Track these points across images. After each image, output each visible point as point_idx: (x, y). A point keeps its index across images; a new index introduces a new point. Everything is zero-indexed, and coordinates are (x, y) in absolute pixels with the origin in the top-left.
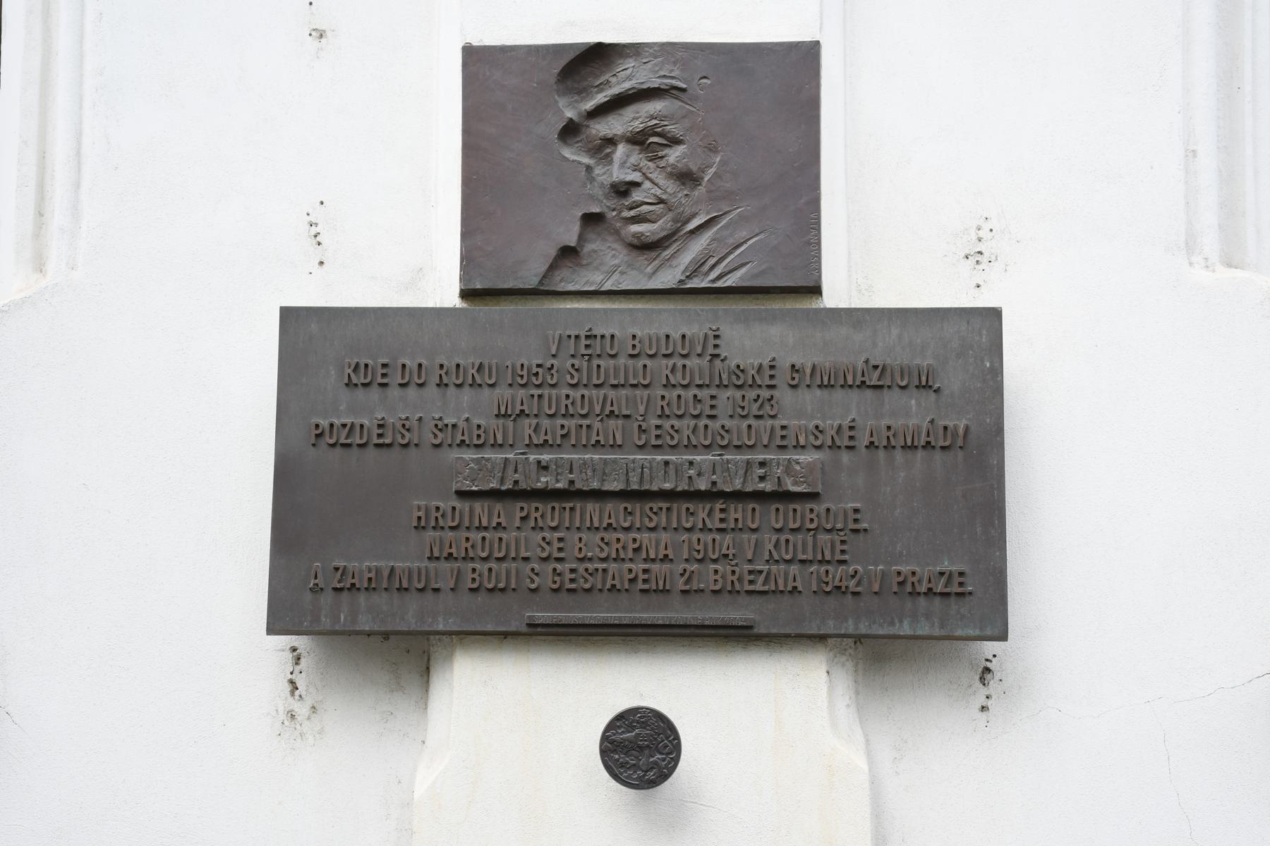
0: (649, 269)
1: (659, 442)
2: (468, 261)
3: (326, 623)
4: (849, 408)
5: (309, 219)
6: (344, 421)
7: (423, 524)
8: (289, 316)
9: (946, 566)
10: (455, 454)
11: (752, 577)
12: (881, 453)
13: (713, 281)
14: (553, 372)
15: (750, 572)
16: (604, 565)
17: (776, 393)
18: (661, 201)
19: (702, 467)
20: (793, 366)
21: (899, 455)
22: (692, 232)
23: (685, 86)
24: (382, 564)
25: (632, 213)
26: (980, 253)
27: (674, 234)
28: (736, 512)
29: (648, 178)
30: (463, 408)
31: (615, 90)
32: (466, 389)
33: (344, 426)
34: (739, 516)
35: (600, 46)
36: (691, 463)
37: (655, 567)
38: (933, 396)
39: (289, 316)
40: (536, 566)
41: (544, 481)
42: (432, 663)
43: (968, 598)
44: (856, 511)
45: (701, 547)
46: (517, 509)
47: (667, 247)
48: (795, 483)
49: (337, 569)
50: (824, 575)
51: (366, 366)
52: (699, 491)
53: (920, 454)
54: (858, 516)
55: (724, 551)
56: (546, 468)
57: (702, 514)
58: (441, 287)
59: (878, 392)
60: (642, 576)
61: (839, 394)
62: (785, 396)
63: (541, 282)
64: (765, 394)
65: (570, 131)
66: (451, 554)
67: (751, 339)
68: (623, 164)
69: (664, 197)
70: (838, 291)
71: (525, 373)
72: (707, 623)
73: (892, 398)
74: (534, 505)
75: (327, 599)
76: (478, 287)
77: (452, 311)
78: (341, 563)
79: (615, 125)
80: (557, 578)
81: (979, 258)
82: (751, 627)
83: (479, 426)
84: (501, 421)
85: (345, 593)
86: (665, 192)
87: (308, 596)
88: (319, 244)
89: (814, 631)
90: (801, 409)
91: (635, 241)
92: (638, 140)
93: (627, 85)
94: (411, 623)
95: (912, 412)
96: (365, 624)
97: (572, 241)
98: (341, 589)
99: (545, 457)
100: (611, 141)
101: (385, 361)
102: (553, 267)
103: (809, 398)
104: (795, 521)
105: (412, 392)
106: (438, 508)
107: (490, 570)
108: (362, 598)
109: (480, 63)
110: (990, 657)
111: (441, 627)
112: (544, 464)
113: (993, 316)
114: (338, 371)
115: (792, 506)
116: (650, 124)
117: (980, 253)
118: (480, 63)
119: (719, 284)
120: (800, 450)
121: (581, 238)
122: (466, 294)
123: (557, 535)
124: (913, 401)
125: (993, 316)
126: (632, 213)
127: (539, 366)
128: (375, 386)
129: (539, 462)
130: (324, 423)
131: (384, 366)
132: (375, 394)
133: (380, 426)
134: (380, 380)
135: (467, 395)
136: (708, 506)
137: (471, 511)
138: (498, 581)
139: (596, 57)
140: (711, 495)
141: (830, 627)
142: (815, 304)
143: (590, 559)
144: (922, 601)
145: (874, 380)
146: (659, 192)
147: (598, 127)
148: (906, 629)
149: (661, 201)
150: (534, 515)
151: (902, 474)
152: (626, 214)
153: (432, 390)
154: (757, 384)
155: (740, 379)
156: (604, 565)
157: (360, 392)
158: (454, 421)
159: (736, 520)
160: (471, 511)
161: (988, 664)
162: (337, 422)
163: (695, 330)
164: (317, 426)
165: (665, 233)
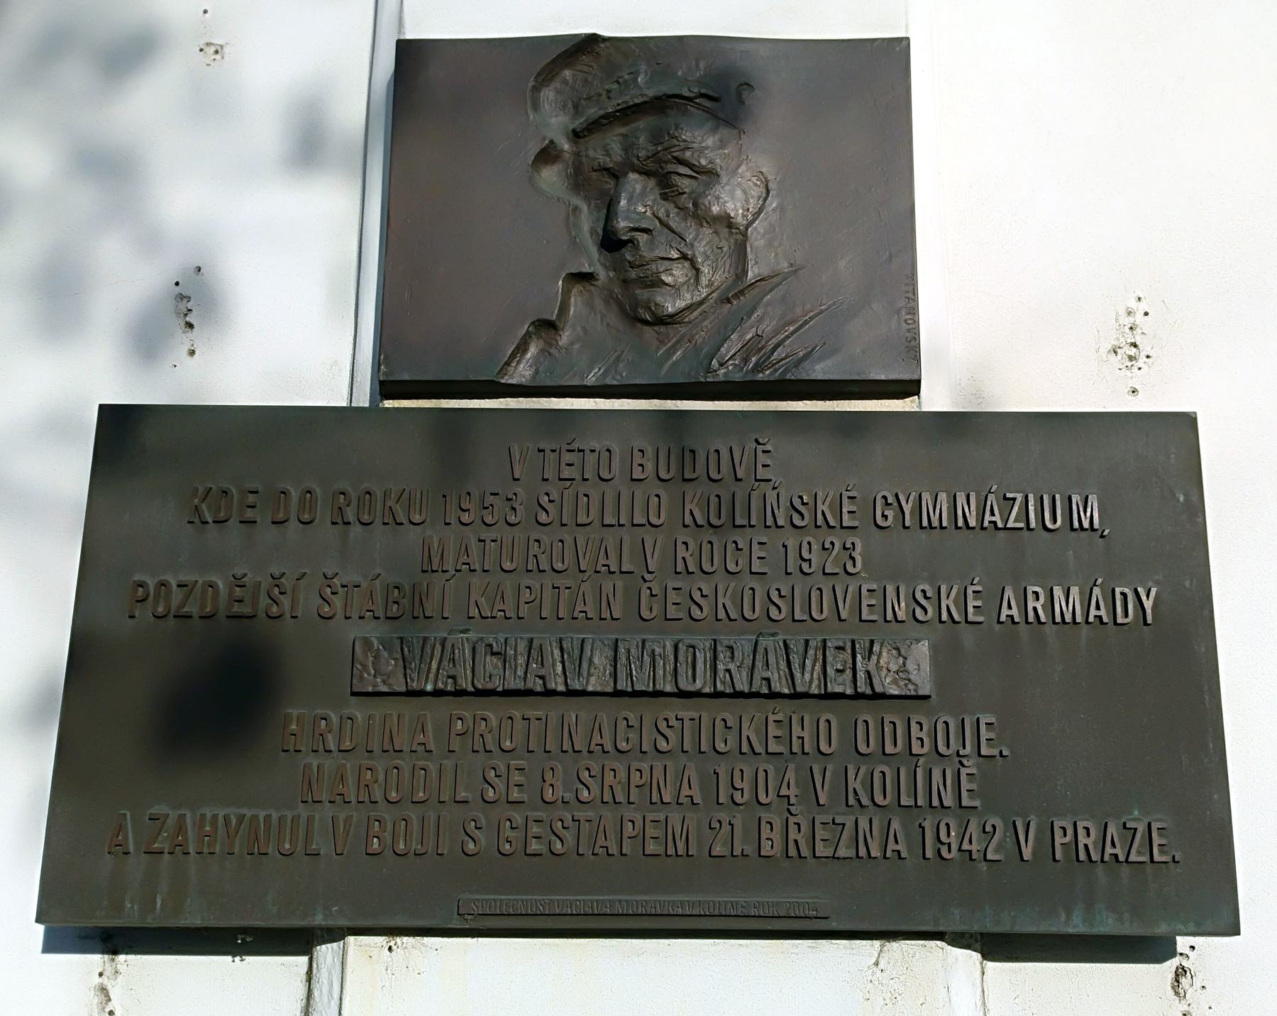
6: (183, 578)
45: (746, 786)
81: (1133, 351)
113: (1186, 424)
117: (1135, 345)
122: (386, 388)
125: (1186, 424)
128: (233, 522)
152: (633, 274)
156: (590, 814)
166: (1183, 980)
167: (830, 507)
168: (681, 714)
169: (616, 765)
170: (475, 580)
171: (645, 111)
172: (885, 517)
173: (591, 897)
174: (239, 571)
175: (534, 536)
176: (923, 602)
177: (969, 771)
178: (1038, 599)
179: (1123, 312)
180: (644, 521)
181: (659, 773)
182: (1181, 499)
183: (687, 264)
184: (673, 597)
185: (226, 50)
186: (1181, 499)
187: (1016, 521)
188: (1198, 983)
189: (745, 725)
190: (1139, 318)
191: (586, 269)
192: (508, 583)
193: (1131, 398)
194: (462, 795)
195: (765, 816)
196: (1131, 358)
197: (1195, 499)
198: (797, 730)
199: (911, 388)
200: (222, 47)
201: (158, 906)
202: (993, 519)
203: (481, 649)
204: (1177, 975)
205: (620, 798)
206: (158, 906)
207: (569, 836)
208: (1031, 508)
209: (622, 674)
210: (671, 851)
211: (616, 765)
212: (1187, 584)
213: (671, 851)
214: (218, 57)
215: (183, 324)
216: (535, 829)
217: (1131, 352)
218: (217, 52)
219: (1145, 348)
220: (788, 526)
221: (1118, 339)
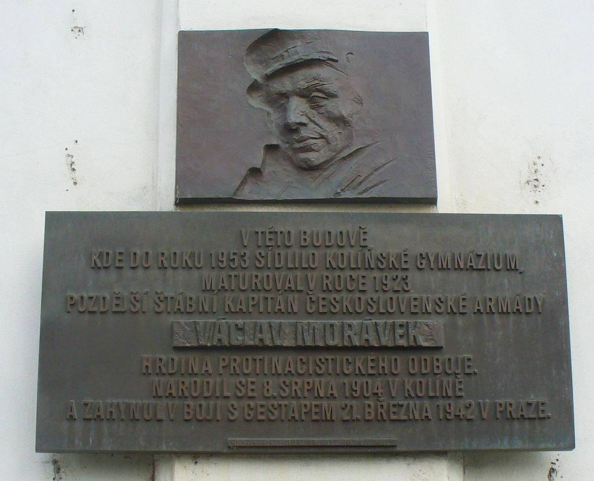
0: (313, 185)
1: (325, 310)
2: (181, 178)
3: (79, 444)
4: (462, 286)
5: (67, 152)
6: (91, 294)
7: (150, 371)
8: (46, 212)
9: (532, 399)
10: (172, 319)
11: (395, 410)
12: (485, 317)
13: (361, 193)
14: (245, 258)
15: (394, 406)
16: (286, 402)
17: (409, 274)
18: (322, 137)
19: (357, 330)
20: (421, 255)
21: (497, 318)
22: (344, 158)
23: (336, 59)
24: (120, 401)
25: (301, 145)
26: (537, 180)
27: (332, 159)
28: (385, 361)
29: (311, 121)
30: (179, 284)
31: (288, 61)
32: (181, 271)
33: (91, 298)
34: (386, 365)
35: (275, 31)
36: (350, 326)
37: (325, 403)
38: (519, 276)
39: (46, 212)
40: (234, 403)
41: (238, 339)
42: (156, 473)
43: (547, 421)
44: (469, 360)
45: (358, 389)
46: (210, 359)
47: (326, 169)
48: (426, 340)
49: (86, 405)
50: (447, 407)
51: (108, 254)
52: (318, 346)
53: (512, 318)
54: (470, 364)
55: (376, 391)
56: (241, 329)
57: (359, 364)
58: (161, 197)
59: (481, 273)
60: (314, 410)
61: (453, 276)
62: (415, 277)
63: (235, 194)
64: (401, 274)
65: (254, 87)
66: (171, 394)
67: (387, 237)
68: (297, 111)
69: (324, 134)
70: (448, 202)
71: (224, 259)
72: (362, 444)
73: (491, 277)
74: (233, 357)
75: (78, 426)
76: (189, 196)
77: (172, 213)
78: (89, 400)
79: (286, 84)
80: (251, 412)
81: (536, 183)
82: (395, 446)
83: (191, 298)
84: (208, 295)
85: (93, 422)
86: (325, 131)
87: (66, 425)
88: (74, 170)
89: (440, 448)
90: (425, 285)
91: (304, 165)
92: (305, 94)
93: (296, 57)
94: (140, 445)
95: (505, 288)
96: (108, 445)
97: (258, 164)
98: (89, 419)
99: (240, 322)
100: (285, 96)
101: (122, 250)
102: (244, 182)
103: (434, 278)
104: (426, 368)
105: (140, 272)
106: (161, 360)
107: (200, 405)
108: (105, 426)
109: (191, 45)
110: (555, 461)
111: (164, 448)
112: (239, 326)
113: (557, 220)
114: (82, 249)
115: (423, 357)
116: (313, 83)
117: (537, 180)
118: (191, 45)
119: (365, 196)
120: (426, 316)
121: (264, 162)
122: (181, 202)
123: (250, 379)
124: (505, 279)
125: (557, 220)
126: (301, 145)
127: (234, 254)
128: (112, 268)
129: (237, 325)
130: (76, 296)
131: (121, 254)
132: (113, 275)
133: (118, 298)
134: (118, 265)
135: (181, 275)
136: (363, 357)
137: (187, 362)
138: (208, 413)
139: (273, 37)
140: (367, 349)
141: (452, 445)
142: (432, 210)
143: (274, 398)
144: (516, 425)
145: (480, 265)
146: (319, 130)
147: (275, 85)
148: (506, 445)
149: (322, 137)
150: (233, 364)
151: (501, 333)
152: (297, 145)
153: (155, 273)
154: (393, 266)
155: (383, 263)
156: (286, 402)
157: (103, 273)
158: (172, 294)
159: (383, 367)
160: (187, 362)
161: (554, 467)
162: (85, 296)
163: (350, 228)
164: (72, 298)
165: (325, 159)
166: (553, 474)
167: (396, 259)
168: (327, 357)
169: (297, 380)
170: (227, 294)
171: (277, 59)
172: (421, 264)
173: (258, 439)
174: (117, 291)
175: (255, 273)
176: (439, 303)
177: (460, 380)
178: (491, 301)
179: (531, 163)
180: (307, 266)
181: (317, 384)
182: (555, 255)
183: (323, 140)
184: (322, 303)
185: (85, 30)
186: (555, 255)
187: (482, 265)
188: (559, 475)
189: (357, 361)
190: (539, 167)
191: (275, 142)
192: (242, 296)
193: (535, 206)
194: (226, 394)
195: (367, 402)
196: (535, 186)
197: (561, 255)
198: (381, 364)
199: (433, 201)
200: (82, 28)
201: (91, 442)
202: (471, 264)
203: (233, 329)
204: (550, 472)
205: (299, 394)
206: (91, 442)
207: (276, 412)
208: (297, 259)
209: (300, 337)
210: (411, 417)
211: (297, 380)
212: (557, 294)
213: (411, 417)
214: (80, 33)
215: (70, 169)
216: (260, 410)
217: (535, 183)
218: (80, 31)
219: (542, 181)
220: (337, 269)
221: (529, 177)
